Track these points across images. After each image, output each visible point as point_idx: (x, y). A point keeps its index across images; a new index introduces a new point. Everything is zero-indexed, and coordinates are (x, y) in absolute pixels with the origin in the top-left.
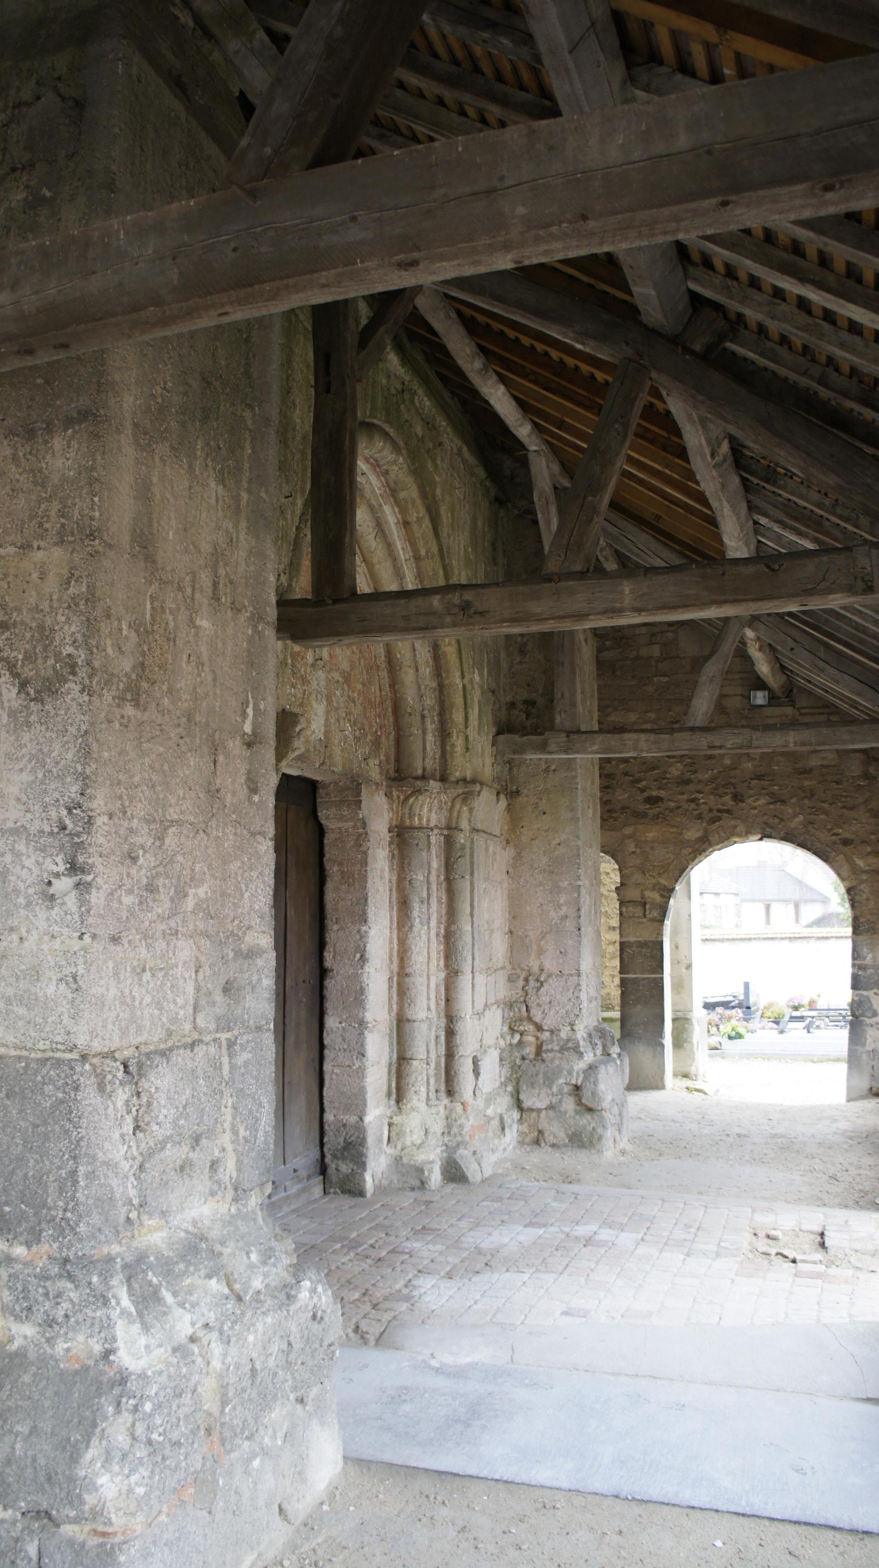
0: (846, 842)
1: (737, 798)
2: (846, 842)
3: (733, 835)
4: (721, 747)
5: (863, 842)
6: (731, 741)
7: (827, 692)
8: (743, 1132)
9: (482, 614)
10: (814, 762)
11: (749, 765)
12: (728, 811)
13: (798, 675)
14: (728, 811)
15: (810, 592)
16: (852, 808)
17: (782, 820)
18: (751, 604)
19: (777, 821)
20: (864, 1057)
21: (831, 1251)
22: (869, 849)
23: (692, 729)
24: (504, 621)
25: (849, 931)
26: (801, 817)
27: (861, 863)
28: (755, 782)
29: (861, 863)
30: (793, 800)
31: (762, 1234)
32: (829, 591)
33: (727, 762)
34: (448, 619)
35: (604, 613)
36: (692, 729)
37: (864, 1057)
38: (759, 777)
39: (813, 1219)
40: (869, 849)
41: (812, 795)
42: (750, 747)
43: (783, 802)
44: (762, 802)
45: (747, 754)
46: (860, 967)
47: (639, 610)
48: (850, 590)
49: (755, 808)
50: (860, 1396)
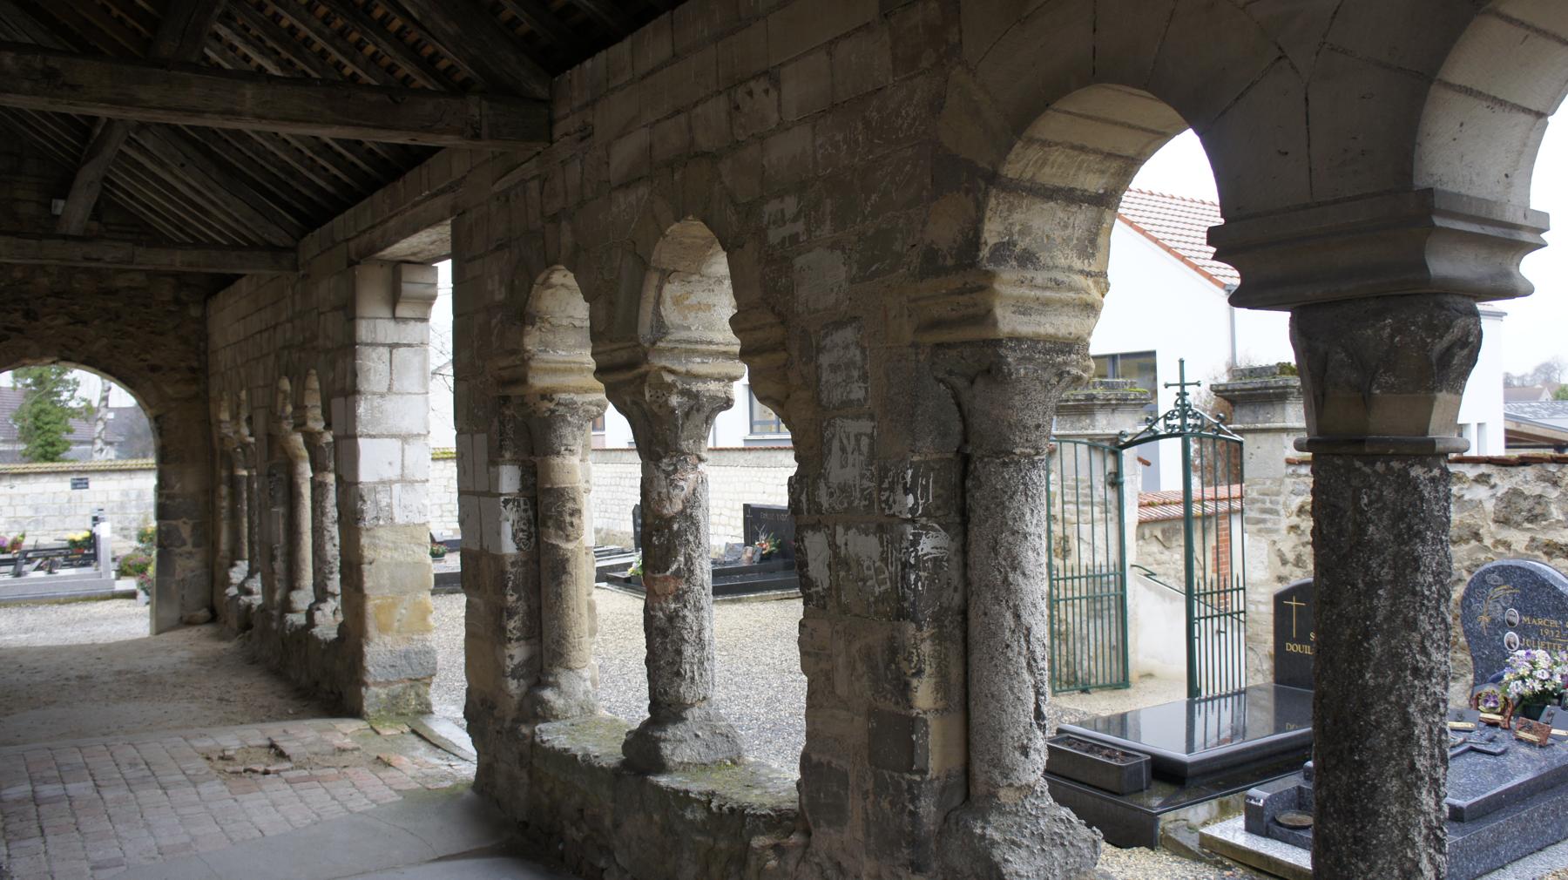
0: (154, 369)
1: (30, 315)
2: (154, 369)
3: (25, 356)
4: (98, 260)
5: (173, 369)
6: (110, 254)
7: (151, 209)
8: (83, 673)
9: (73, 87)
10: (121, 282)
11: (45, 281)
12: (19, 330)
13: (119, 188)
14: (19, 330)
15: (427, 129)
16: (162, 334)
17: (83, 342)
18: (371, 131)
19: (77, 343)
20: (174, 587)
21: (294, 759)
22: (178, 376)
23: (65, 237)
24: (101, 100)
25: (151, 461)
26: (105, 341)
27: (169, 391)
28: (51, 300)
29: (169, 391)
30: (97, 322)
31: (215, 757)
32: (442, 132)
33: (18, 274)
34: (27, 85)
35: (222, 113)
36: (65, 237)
37: (174, 587)
38: (57, 295)
39: (256, 735)
40: (178, 376)
41: (118, 317)
42: (131, 262)
43: (85, 323)
44: (60, 321)
45: (42, 267)
46: (168, 497)
47: (260, 117)
48: (460, 133)
49: (51, 328)
50: (454, 852)
